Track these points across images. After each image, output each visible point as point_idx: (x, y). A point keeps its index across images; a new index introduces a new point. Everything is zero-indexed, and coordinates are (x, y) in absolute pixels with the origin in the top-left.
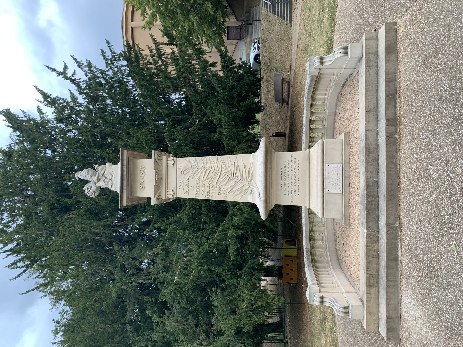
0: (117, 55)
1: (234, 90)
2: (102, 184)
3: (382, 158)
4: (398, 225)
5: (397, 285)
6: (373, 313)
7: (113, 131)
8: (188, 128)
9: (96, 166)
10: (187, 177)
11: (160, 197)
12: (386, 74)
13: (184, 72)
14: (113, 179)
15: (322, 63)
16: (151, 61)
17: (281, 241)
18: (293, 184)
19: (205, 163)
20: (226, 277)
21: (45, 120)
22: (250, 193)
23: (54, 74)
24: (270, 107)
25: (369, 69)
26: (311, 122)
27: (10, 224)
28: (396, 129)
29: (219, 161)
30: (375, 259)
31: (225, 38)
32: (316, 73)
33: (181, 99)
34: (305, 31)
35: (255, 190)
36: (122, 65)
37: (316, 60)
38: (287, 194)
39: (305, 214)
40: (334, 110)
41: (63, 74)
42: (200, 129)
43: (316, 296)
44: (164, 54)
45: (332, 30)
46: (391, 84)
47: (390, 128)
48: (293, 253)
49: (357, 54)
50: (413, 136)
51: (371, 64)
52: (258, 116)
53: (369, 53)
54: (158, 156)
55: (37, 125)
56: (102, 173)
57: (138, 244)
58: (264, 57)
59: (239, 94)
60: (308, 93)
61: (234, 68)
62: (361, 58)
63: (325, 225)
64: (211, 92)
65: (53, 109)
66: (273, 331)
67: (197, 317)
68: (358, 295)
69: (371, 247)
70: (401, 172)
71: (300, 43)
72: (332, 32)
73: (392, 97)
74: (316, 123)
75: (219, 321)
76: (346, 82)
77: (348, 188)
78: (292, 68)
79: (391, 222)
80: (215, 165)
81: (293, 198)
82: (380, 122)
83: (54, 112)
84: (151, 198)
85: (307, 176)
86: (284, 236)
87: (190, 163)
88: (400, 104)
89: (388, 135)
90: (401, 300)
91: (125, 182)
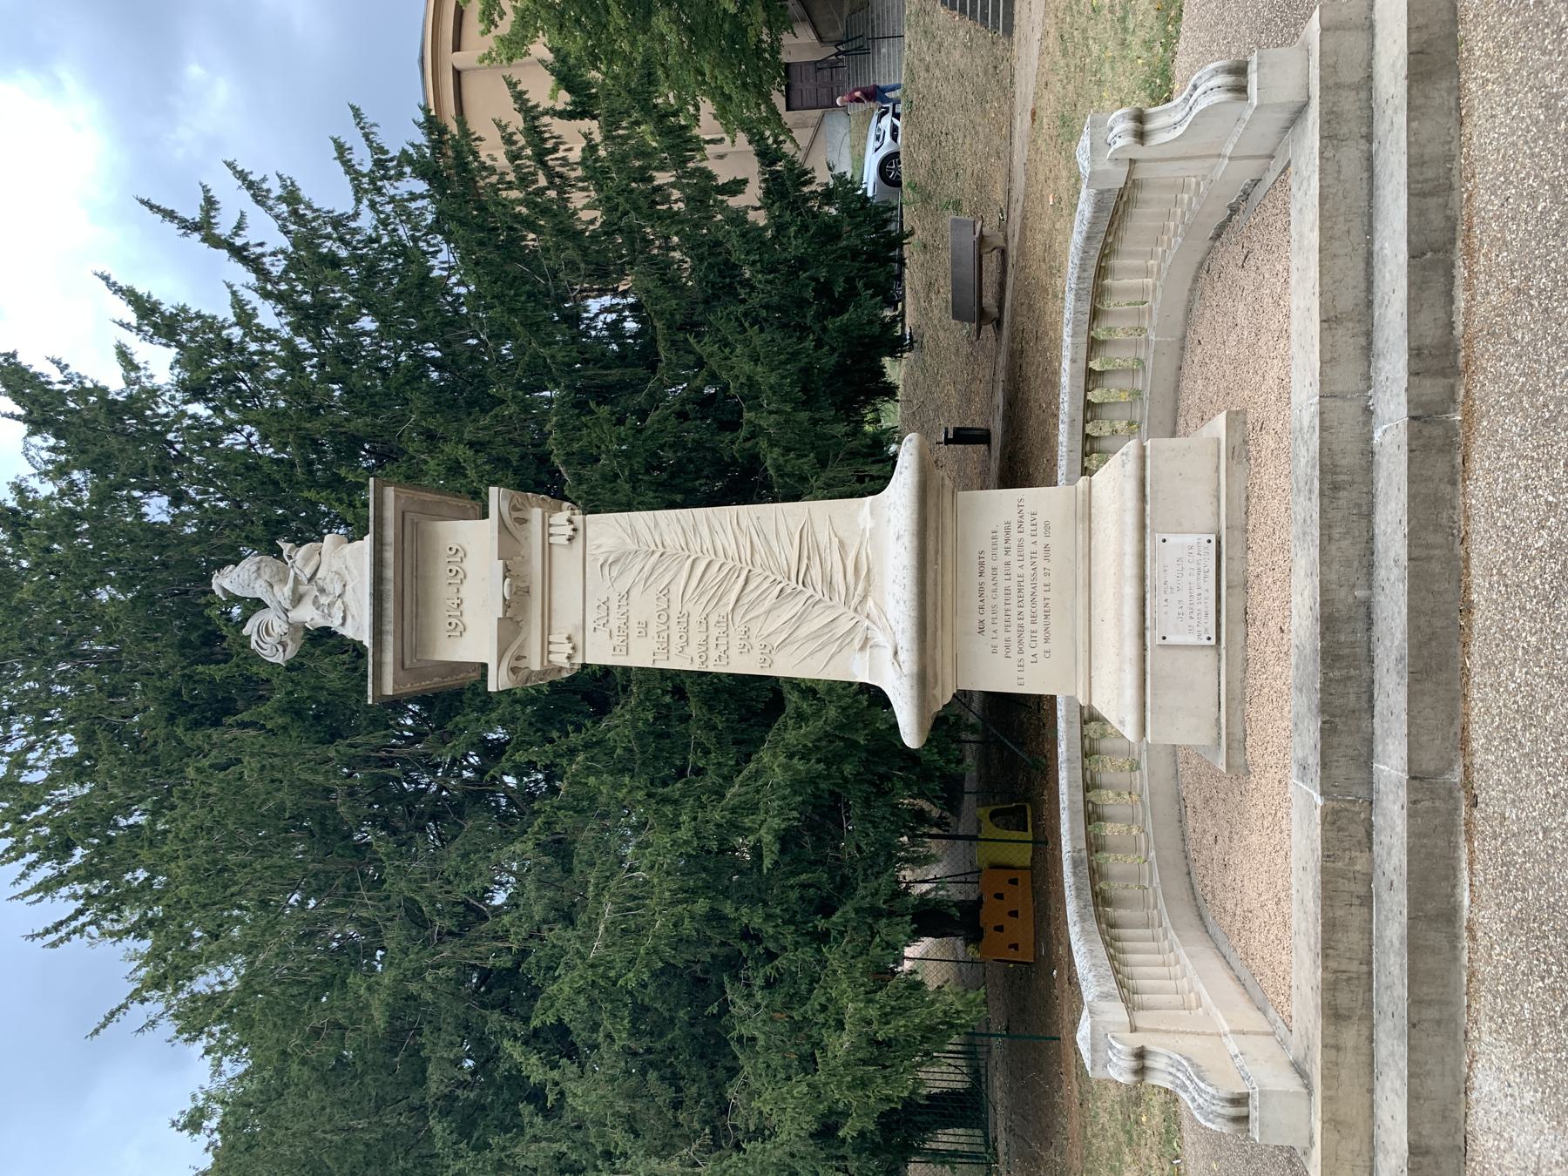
0: (391, 160)
1: (803, 275)
2: (308, 615)
3: (1392, 505)
4: (1456, 777)
5: (1453, 1019)
6: (1350, 1126)
7: (374, 426)
8: (642, 414)
9: (286, 547)
10: (623, 585)
11: (522, 664)
12: (1409, 166)
13: (626, 213)
14: (348, 597)
15: (1141, 136)
16: (511, 177)
17: (973, 811)
18: (1027, 610)
19: (690, 534)
20: (776, 940)
21: (143, 389)
22: (862, 648)
23: (173, 227)
24: (936, 340)
25: (1336, 148)
26: (1092, 377)
27: (31, 756)
28: (1452, 391)
29: (743, 526)
30: (1359, 912)
31: (779, 100)
32: (1118, 178)
33: (620, 312)
34: (1065, 54)
35: (879, 637)
36: (411, 193)
37: (1119, 125)
38: (1001, 650)
39: (1069, 722)
40: (1178, 333)
41: (203, 227)
42: (682, 416)
43: (1119, 1046)
44: (555, 150)
45: (1168, 36)
46: (1432, 202)
47: (1427, 382)
48: (1020, 855)
49: (1286, 91)
50: (1532, 411)
51: (1345, 130)
52: (895, 370)
53: (1338, 86)
54: (514, 508)
55: (111, 408)
56: (308, 572)
57: (470, 823)
58: (914, 164)
59: (823, 290)
60: (1083, 268)
61: (807, 200)
62: (1301, 111)
63: (1144, 765)
64: (722, 281)
65: (173, 353)
66: (949, 1121)
67: (674, 1080)
68: (1282, 1043)
69: (1340, 865)
70: (1474, 561)
71: (1043, 103)
72: (1170, 42)
73: (1436, 256)
74: (1108, 381)
75: (754, 1094)
76: (1230, 218)
77: (1243, 625)
78: (1014, 198)
79: (1429, 764)
80: (726, 541)
81: (1027, 663)
82: (1381, 363)
83: (177, 361)
84: (485, 666)
85: (1080, 583)
86: (984, 797)
87: (635, 534)
88: (1469, 286)
89: (1420, 412)
90: (1468, 1078)
91: (390, 607)
